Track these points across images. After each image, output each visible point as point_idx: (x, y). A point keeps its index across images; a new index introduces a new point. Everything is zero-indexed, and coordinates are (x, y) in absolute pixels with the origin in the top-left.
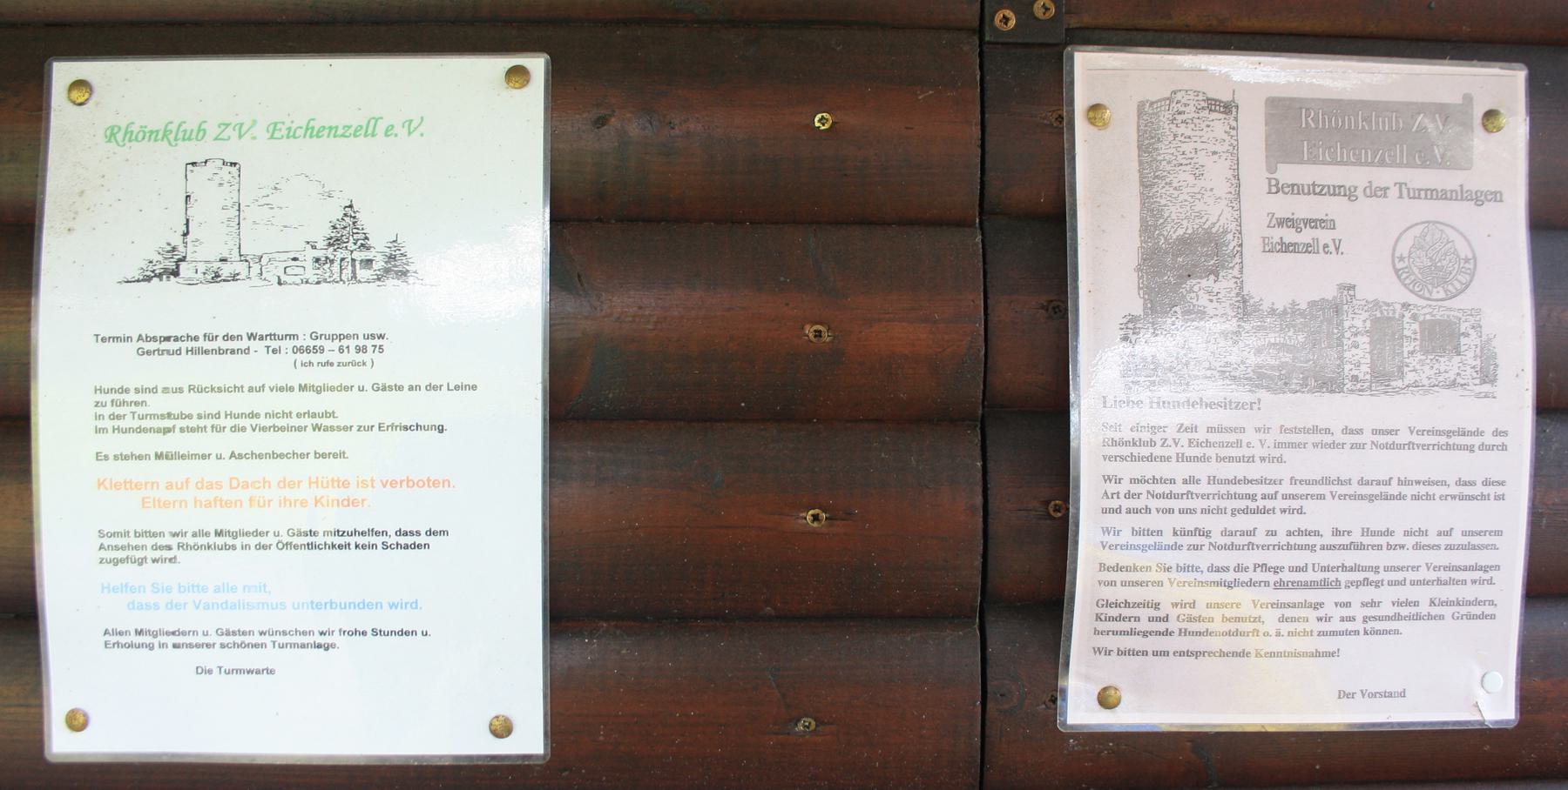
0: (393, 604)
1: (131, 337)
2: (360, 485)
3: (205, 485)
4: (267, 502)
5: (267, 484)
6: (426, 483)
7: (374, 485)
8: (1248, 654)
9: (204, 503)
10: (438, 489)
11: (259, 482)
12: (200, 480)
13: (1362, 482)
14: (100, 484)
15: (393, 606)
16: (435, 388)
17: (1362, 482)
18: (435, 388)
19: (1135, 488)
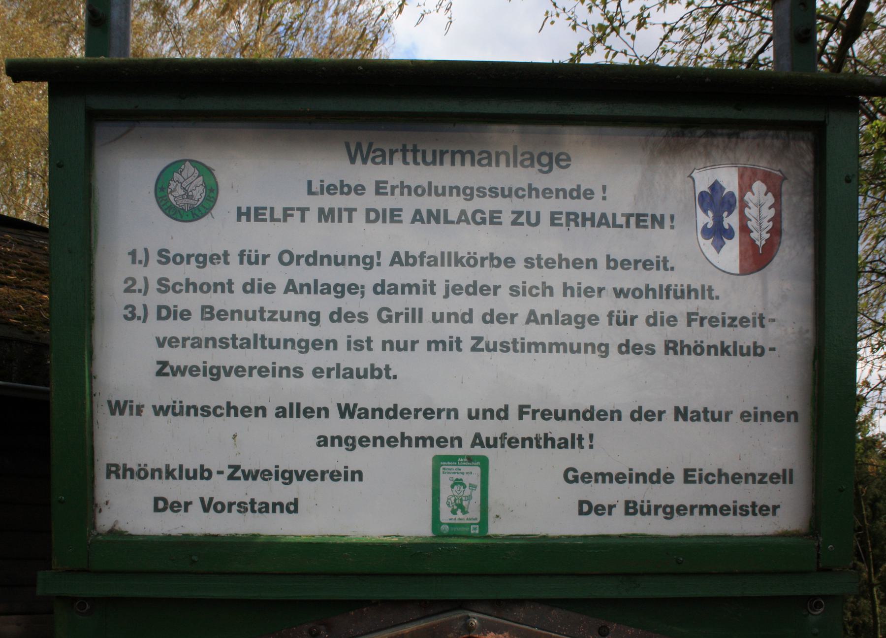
0: (161, 407)
1: (619, 412)
2: (353, 346)
3: (387, 288)
4: (185, 409)
5: (548, 291)
6: (384, 372)
7: (764, 323)
8: (745, 416)
9: (557, 442)
10: (766, 517)
11: (537, 288)
12: (624, 342)
13: (235, 473)
14: (604, 198)
15: (261, 410)
16: (650, 416)
17: (235, 473)
18: (650, 416)
19: (627, 305)
